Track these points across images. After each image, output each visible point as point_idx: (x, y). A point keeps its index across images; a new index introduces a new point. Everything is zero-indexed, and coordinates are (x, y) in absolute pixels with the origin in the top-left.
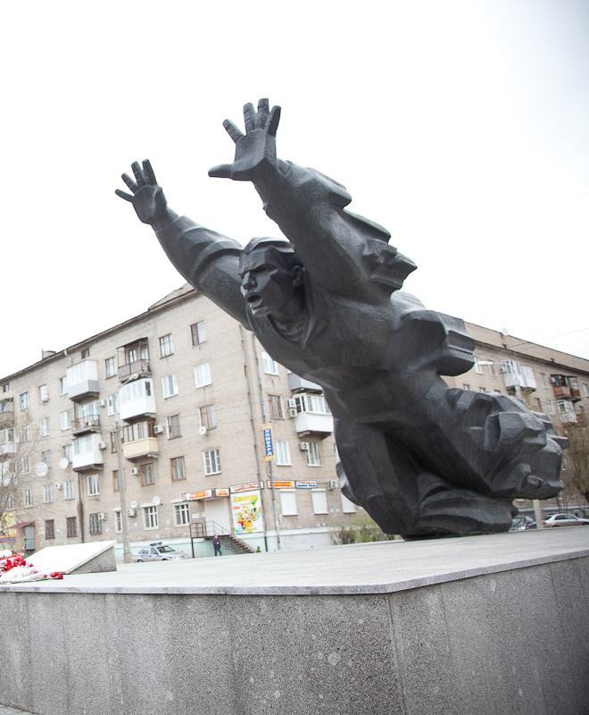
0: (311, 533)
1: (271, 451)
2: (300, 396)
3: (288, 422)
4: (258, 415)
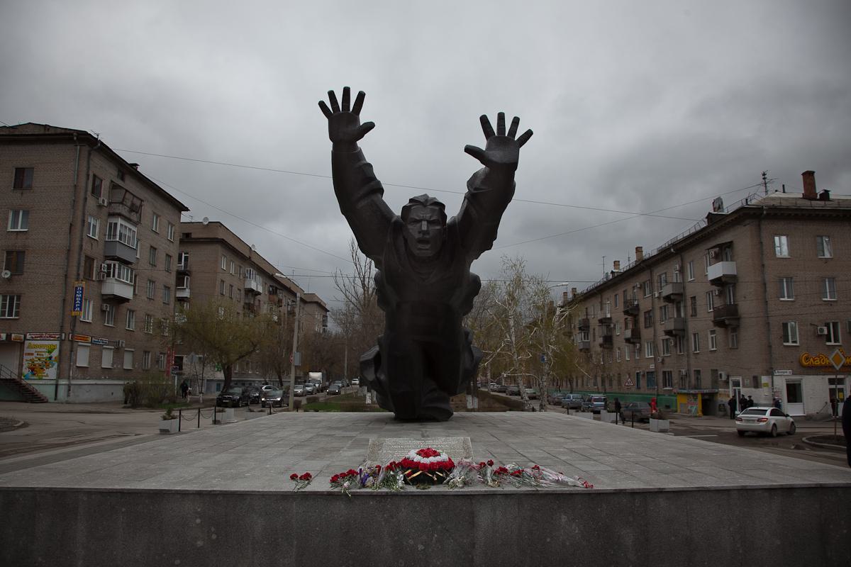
0: (96, 384)
1: (80, 307)
2: (112, 263)
3: (96, 283)
4: (73, 271)
